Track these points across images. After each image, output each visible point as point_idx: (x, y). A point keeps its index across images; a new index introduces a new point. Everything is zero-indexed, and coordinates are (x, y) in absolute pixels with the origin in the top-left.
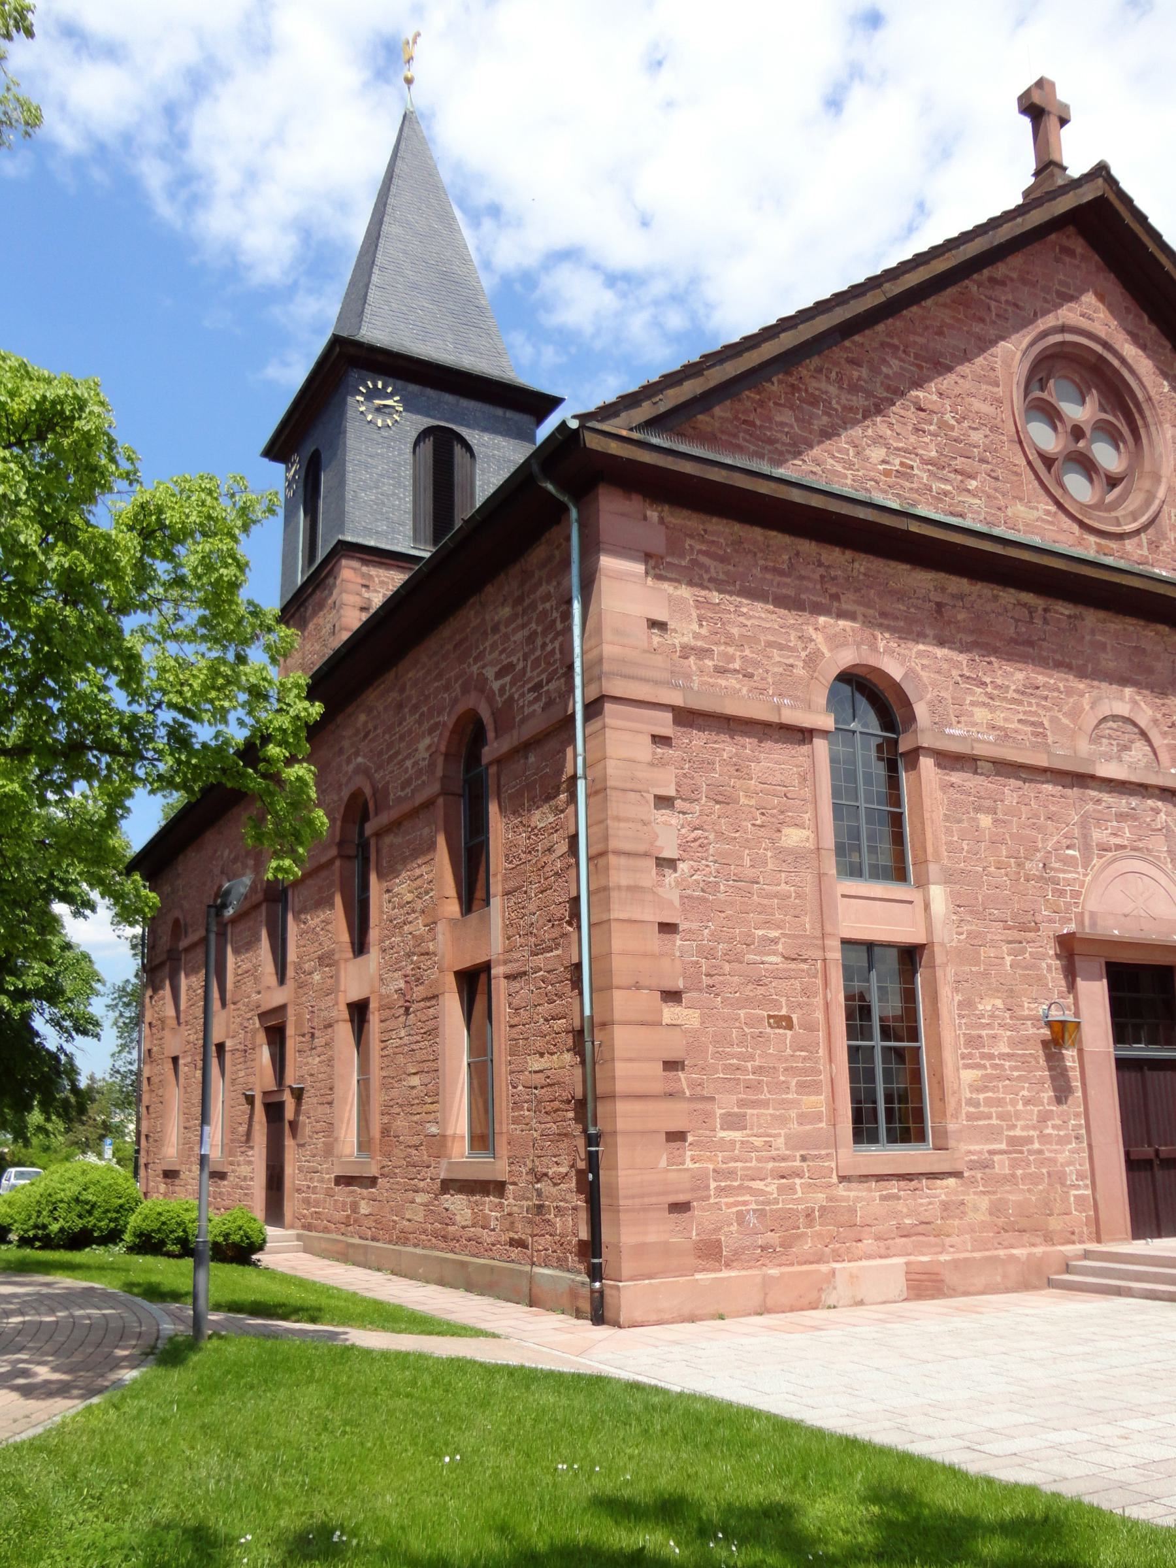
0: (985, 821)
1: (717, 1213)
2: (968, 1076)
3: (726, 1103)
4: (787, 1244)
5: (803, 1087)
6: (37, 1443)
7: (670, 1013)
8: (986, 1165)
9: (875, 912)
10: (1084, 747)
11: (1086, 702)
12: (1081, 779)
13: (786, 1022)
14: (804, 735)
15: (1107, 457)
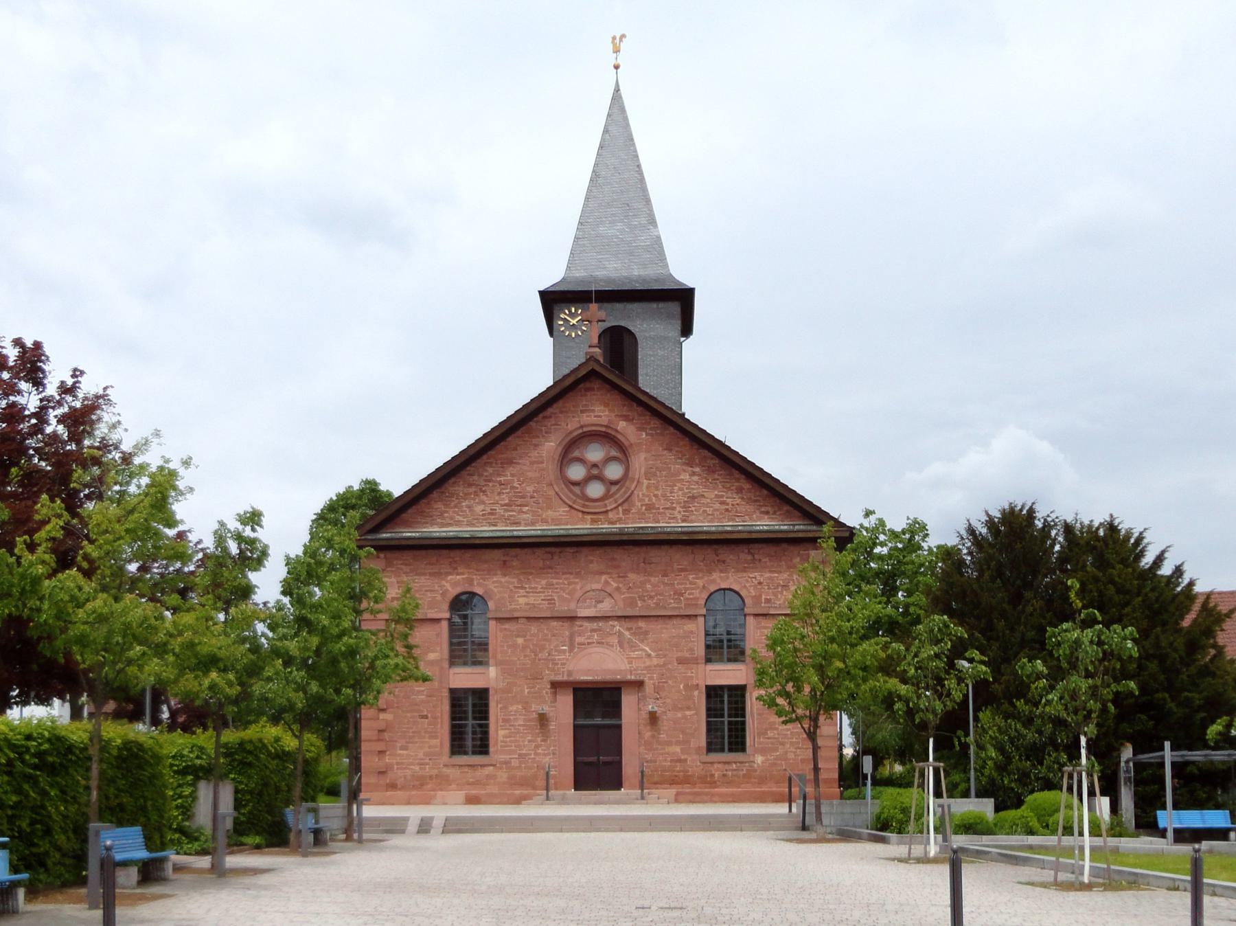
0: (520, 641)
1: (398, 774)
2: (501, 733)
3: (401, 742)
4: (422, 785)
5: (431, 737)
6: (249, 747)
7: (382, 716)
8: (507, 763)
9: (465, 678)
10: (573, 605)
11: (578, 587)
12: (573, 619)
13: (426, 717)
14: (438, 620)
15: (614, 471)
